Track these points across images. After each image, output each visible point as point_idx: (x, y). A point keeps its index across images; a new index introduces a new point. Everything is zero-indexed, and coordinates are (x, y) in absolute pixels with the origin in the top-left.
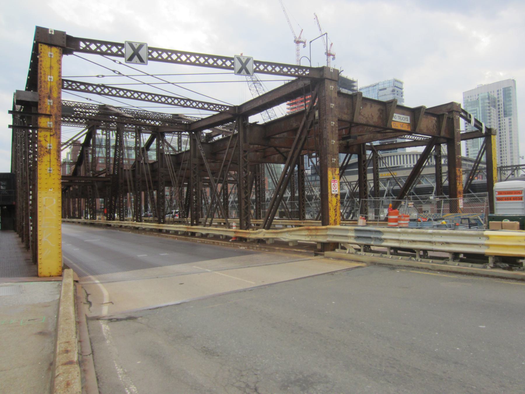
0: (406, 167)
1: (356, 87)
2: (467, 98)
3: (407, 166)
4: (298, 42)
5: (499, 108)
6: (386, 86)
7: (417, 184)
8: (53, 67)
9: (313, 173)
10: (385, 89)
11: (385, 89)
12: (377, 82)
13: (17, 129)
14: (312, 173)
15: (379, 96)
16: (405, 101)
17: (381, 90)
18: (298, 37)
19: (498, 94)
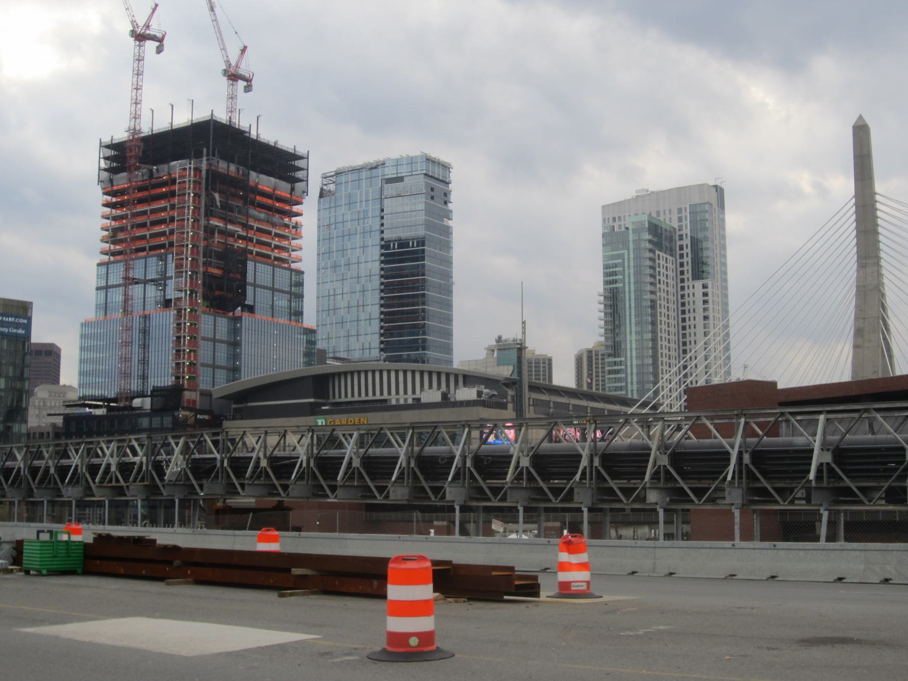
0: (394, 402)
1: (306, 171)
2: (611, 220)
3: (398, 400)
5: (682, 256)
6: (403, 171)
10: (400, 179)
11: (400, 179)
12: (381, 158)
16: (454, 215)
17: (390, 181)
18: (141, 23)
19: (680, 219)
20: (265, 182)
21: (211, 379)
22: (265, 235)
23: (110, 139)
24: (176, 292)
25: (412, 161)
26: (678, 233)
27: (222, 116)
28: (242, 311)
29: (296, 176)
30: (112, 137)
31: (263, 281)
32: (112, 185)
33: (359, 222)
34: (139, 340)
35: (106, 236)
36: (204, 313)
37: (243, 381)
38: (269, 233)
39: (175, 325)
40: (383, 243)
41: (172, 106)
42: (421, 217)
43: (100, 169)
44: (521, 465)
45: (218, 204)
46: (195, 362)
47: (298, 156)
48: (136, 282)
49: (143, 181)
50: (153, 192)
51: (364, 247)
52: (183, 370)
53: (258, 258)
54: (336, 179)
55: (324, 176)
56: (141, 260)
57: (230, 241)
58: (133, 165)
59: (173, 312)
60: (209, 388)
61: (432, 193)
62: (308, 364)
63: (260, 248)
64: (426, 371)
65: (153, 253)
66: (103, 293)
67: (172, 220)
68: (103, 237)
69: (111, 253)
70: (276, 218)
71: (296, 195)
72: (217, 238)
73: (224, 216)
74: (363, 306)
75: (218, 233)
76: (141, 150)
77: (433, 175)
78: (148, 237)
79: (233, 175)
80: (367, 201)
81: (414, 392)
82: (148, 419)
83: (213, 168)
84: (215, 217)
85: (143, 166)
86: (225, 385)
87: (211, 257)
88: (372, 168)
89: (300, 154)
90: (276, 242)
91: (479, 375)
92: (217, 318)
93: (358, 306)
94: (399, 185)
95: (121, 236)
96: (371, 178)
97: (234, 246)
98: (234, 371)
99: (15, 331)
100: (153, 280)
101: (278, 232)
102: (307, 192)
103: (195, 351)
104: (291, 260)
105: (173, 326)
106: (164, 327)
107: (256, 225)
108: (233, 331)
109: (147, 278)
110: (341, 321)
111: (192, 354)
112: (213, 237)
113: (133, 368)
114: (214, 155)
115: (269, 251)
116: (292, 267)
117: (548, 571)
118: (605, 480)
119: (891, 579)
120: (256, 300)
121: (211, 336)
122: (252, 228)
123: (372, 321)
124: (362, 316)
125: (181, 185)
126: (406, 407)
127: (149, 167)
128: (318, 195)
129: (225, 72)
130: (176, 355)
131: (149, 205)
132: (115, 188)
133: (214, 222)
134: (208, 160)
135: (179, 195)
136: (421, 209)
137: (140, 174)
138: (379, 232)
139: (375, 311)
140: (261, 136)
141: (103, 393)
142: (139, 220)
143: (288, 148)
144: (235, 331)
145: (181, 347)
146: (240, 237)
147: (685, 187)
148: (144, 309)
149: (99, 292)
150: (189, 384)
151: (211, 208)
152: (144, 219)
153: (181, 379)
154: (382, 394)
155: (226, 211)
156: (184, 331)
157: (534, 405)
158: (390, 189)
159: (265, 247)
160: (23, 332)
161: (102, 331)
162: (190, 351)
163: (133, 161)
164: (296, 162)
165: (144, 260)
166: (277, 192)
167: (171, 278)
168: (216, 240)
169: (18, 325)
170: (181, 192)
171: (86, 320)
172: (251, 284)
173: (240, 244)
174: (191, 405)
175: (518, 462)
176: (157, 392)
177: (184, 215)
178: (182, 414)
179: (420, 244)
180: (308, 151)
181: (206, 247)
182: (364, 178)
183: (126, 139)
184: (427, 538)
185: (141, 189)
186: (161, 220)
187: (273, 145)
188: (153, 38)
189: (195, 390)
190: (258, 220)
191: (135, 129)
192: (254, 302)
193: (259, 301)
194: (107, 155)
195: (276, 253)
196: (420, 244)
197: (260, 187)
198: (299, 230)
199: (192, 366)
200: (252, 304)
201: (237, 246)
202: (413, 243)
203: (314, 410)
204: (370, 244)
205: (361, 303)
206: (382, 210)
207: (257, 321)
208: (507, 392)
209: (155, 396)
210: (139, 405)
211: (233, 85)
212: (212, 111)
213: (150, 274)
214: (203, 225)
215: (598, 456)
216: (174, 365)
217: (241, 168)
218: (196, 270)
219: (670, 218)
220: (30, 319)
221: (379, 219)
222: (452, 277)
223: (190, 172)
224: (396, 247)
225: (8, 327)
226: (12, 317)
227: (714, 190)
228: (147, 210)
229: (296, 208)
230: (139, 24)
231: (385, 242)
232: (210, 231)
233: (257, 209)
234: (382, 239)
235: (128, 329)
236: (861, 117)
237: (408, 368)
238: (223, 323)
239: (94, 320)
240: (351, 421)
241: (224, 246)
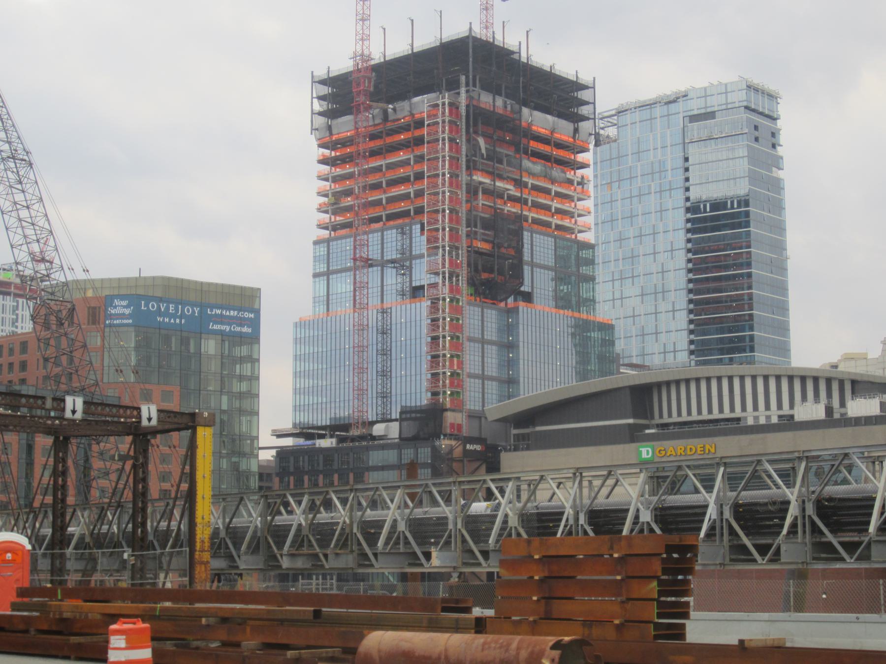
0: (750, 422)
1: (591, 106)
3: (756, 418)
6: (714, 103)
7: (744, 489)
9: (407, 434)
11: (711, 115)
13: (113, 585)
14: (404, 436)
15: (687, 141)
16: (786, 163)
17: (694, 118)
22: (544, 195)
23: (326, 71)
24: (428, 276)
27: (479, 31)
28: (515, 300)
29: (580, 112)
30: (329, 68)
31: (542, 258)
32: (331, 134)
33: (653, 177)
34: (377, 344)
35: (325, 204)
36: (469, 304)
38: (547, 192)
39: (429, 321)
40: (688, 204)
41: (384, 29)
43: (313, 113)
44: (641, 520)
45: (484, 151)
46: (459, 371)
47: (582, 84)
48: (368, 263)
49: (375, 125)
50: (389, 140)
51: (661, 211)
52: (444, 382)
53: (535, 227)
54: (618, 120)
56: (376, 235)
57: (499, 204)
58: (363, 103)
59: (426, 304)
60: (478, 407)
61: (757, 134)
62: (583, 375)
63: (537, 213)
64: (797, 376)
65: (391, 223)
66: (323, 281)
67: (419, 176)
68: (320, 205)
69: (333, 226)
70: (556, 172)
71: (580, 138)
72: (481, 200)
73: (491, 170)
74: (663, 292)
76: (372, 83)
77: (756, 108)
79: (501, 112)
80: (664, 147)
81: (780, 406)
82: (396, 451)
83: (475, 103)
84: (479, 170)
85: (374, 104)
86: (495, 405)
87: (476, 226)
88: (670, 102)
90: (555, 204)
91: (871, 380)
93: (656, 293)
95: (348, 201)
96: (668, 115)
97: (503, 210)
98: (510, 383)
99: (238, 329)
100: (393, 261)
101: (559, 190)
103: (458, 356)
104: (577, 228)
105: (426, 322)
106: (413, 324)
107: (530, 181)
108: (506, 328)
109: (385, 258)
111: (455, 360)
112: (476, 199)
113: (370, 383)
114: (475, 86)
115: (548, 216)
116: (578, 238)
118: (821, 533)
120: (535, 286)
121: (478, 335)
122: (526, 185)
123: (677, 314)
124: (663, 307)
125: (431, 128)
126: (768, 428)
130: (432, 362)
131: (385, 158)
133: (478, 177)
134: (467, 91)
135: (428, 142)
137: (371, 116)
138: (682, 190)
139: (681, 300)
140: (533, 58)
141: (311, 419)
142: (372, 180)
144: (509, 328)
145: (438, 351)
146: (512, 199)
149: (317, 279)
150: (452, 401)
151: (474, 158)
152: (377, 177)
153: (441, 396)
154: (732, 409)
156: (444, 329)
158: (697, 130)
159: (543, 211)
160: (250, 330)
161: (320, 333)
162: (452, 356)
163: (362, 99)
164: (579, 92)
165: (380, 234)
166: (557, 136)
167: (421, 256)
168: (481, 202)
169: (241, 322)
170: (432, 138)
171: (300, 319)
172: (528, 264)
173: (510, 208)
174: (456, 432)
175: (637, 517)
176: (407, 414)
177: (437, 169)
178: (444, 443)
179: (743, 203)
180: (594, 78)
181: (469, 211)
182: (658, 116)
183: (352, 69)
184: (858, 618)
185: (373, 137)
186: (401, 178)
187: (549, 70)
189: (461, 411)
191: (362, 55)
193: (538, 286)
194: (322, 94)
195: (556, 221)
196: (743, 203)
197: (534, 128)
199: (455, 377)
200: (530, 291)
201: (508, 211)
202: (732, 203)
203: (634, 435)
204: (670, 207)
206: (686, 159)
207: (538, 313)
209: (406, 419)
210: (382, 433)
212: (471, 23)
213: (418, 248)
214: (464, 182)
215: (811, 502)
216: (429, 376)
217: (509, 102)
218: (456, 244)
220: (257, 312)
221: (682, 171)
222: (786, 250)
223: (444, 108)
224: (708, 210)
226: (234, 310)
228: (382, 166)
231: (692, 203)
232: (473, 190)
233: (531, 158)
234: (688, 199)
237: (770, 373)
238: (492, 315)
239: (311, 318)
240: (691, 449)
241: (493, 210)
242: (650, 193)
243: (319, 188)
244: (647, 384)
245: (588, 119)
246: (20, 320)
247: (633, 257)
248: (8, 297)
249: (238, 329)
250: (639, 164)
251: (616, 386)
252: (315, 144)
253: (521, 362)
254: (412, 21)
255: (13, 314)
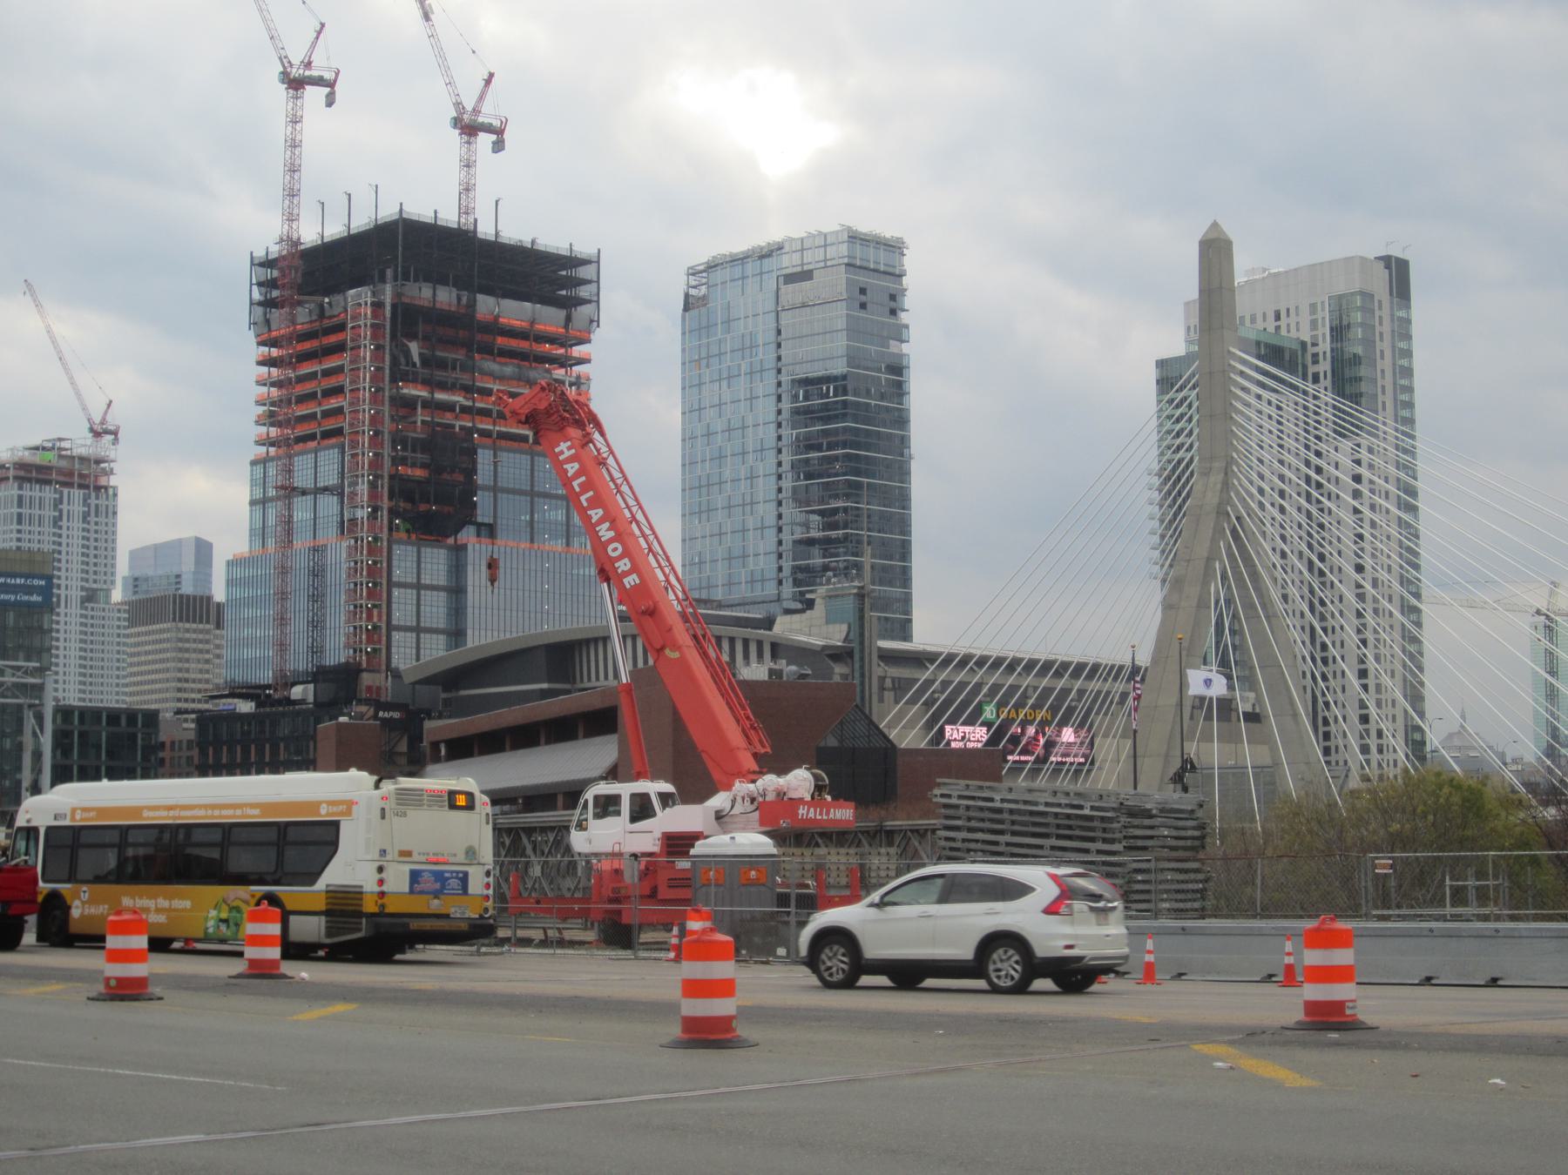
1: (595, 285)
4: (296, 84)
6: (812, 258)
8: (1106, 919)
10: (806, 275)
11: (806, 275)
16: (914, 333)
17: (791, 278)
19: (1314, 324)
20: (514, 312)
21: (414, 651)
23: (264, 253)
25: (825, 241)
26: (1311, 350)
37: (471, 648)
42: (840, 343)
43: (251, 304)
45: (416, 359)
49: (311, 322)
51: (751, 399)
53: (503, 443)
55: (690, 271)
56: (331, 451)
57: (448, 418)
61: (863, 298)
65: (327, 442)
68: (259, 416)
72: (421, 416)
74: (752, 503)
75: (423, 407)
78: (319, 416)
88: (762, 257)
89: (584, 256)
92: (423, 549)
94: (806, 285)
97: (453, 426)
98: (456, 634)
99: (26, 598)
102: (598, 321)
110: (741, 528)
117: (1183, 977)
119: (1501, 979)
120: (499, 514)
123: (767, 532)
127: (320, 298)
128: (682, 307)
129: (457, 122)
132: (274, 334)
133: (411, 391)
136: (839, 328)
143: (558, 248)
147: (1321, 264)
148: (315, 538)
155: (434, 372)
157: (894, 688)
158: (791, 293)
160: (40, 599)
168: (419, 418)
169: (29, 590)
174: (374, 696)
176: (319, 675)
179: (840, 390)
180: (599, 250)
187: (530, 246)
188: (319, 81)
190: (501, 378)
192: (495, 517)
194: (263, 279)
198: (583, 388)
200: (491, 522)
205: (748, 500)
206: (779, 332)
208: (833, 668)
211: (469, 143)
212: (401, 204)
219: (1298, 323)
225: (15, 593)
227: (1382, 264)
229: (577, 351)
230: (293, 62)
233: (498, 359)
235: (284, 571)
236: (1215, 225)
242: (739, 375)
243: (258, 395)
244: (565, 642)
245: (589, 302)
246: (65, 518)
247: (720, 457)
248: (48, 488)
249: (26, 598)
250: (728, 336)
251: (524, 646)
252: (253, 341)
253: (470, 610)
254: (349, 195)
255: (54, 510)
